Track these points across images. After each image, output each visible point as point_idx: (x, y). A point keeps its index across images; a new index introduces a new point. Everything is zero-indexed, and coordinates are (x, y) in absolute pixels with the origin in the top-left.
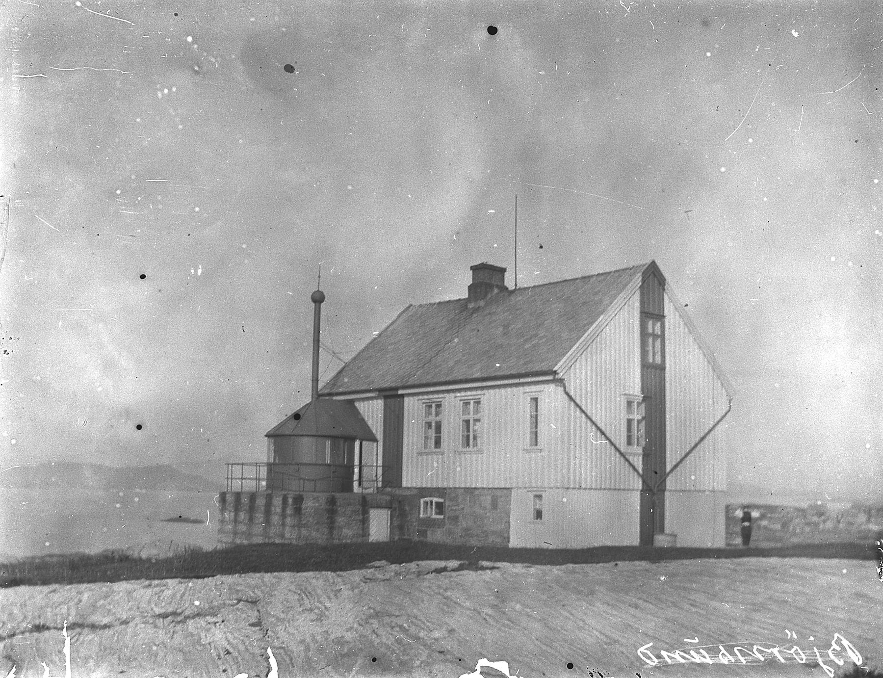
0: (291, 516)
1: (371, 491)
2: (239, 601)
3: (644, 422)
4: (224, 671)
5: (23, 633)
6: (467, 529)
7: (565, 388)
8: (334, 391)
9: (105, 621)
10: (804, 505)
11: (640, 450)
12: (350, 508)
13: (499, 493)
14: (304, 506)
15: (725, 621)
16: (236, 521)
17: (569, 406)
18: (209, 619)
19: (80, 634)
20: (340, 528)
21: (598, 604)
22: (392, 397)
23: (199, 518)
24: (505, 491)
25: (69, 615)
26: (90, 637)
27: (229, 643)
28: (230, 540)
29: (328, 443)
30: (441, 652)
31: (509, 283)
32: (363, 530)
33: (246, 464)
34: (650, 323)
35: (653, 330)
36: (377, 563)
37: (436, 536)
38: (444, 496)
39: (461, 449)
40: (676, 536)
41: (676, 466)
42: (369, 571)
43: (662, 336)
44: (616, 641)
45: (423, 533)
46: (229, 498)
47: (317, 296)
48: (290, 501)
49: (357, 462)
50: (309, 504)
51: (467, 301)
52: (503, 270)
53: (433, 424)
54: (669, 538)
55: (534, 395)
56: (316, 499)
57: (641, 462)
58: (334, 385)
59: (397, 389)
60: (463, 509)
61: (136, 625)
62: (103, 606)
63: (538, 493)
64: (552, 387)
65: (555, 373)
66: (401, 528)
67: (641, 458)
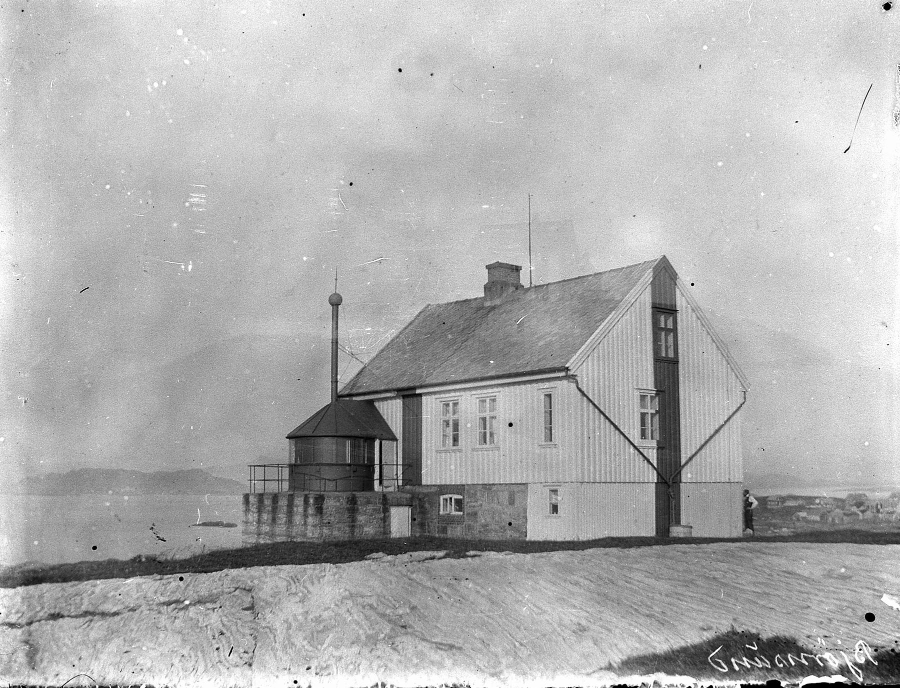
0: (312, 515)
1: (391, 489)
2: (236, 589)
3: (657, 416)
4: (217, 649)
5: (39, 621)
6: (485, 526)
7: (577, 383)
8: (354, 391)
9: (115, 609)
10: (843, 495)
11: (654, 444)
12: (370, 507)
13: (516, 489)
14: (324, 507)
15: (651, 595)
16: (259, 522)
17: (582, 403)
18: (209, 605)
19: (91, 621)
20: (361, 526)
21: (541, 582)
22: (409, 395)
23: (231, 522)
24: (522, 487)
25: (82, 604)
26: (99, 623)
27: (224, 625)
28: (255, 541)
29: (348, 443)
30: (403, 627)
31: (525, 281)
32: (384, 528)
33: (269, 466)
34: (662, 318)
35: (666, 325)
36: (375, 555)
37: (456, 532)
38: (461, 492)
39: (478, 446)
40: (691, 527)
41: (691, 459)
42: (367, 562)
43: (675, 330)
44: (545, 612)
45: (444, 530)
46: (252, 499)
47: (335, 300)
48: (311, 501)
49: (377, 461)
50: (330, 504)
51: (484, 299)
52: (517, 269)
53: (451, 423)
54: (686, 530)
55: (548, 392)
56: (337, 498)
57: (655, 455)
58: (354, 385)
59: (414, 388)
60: (481, 505)
61: (142, 612)
62: (114, 596)
63: (554, 488)
64: (565, 382)
65: (567, 369)
66: (422, 525)
67: (655, 451)
